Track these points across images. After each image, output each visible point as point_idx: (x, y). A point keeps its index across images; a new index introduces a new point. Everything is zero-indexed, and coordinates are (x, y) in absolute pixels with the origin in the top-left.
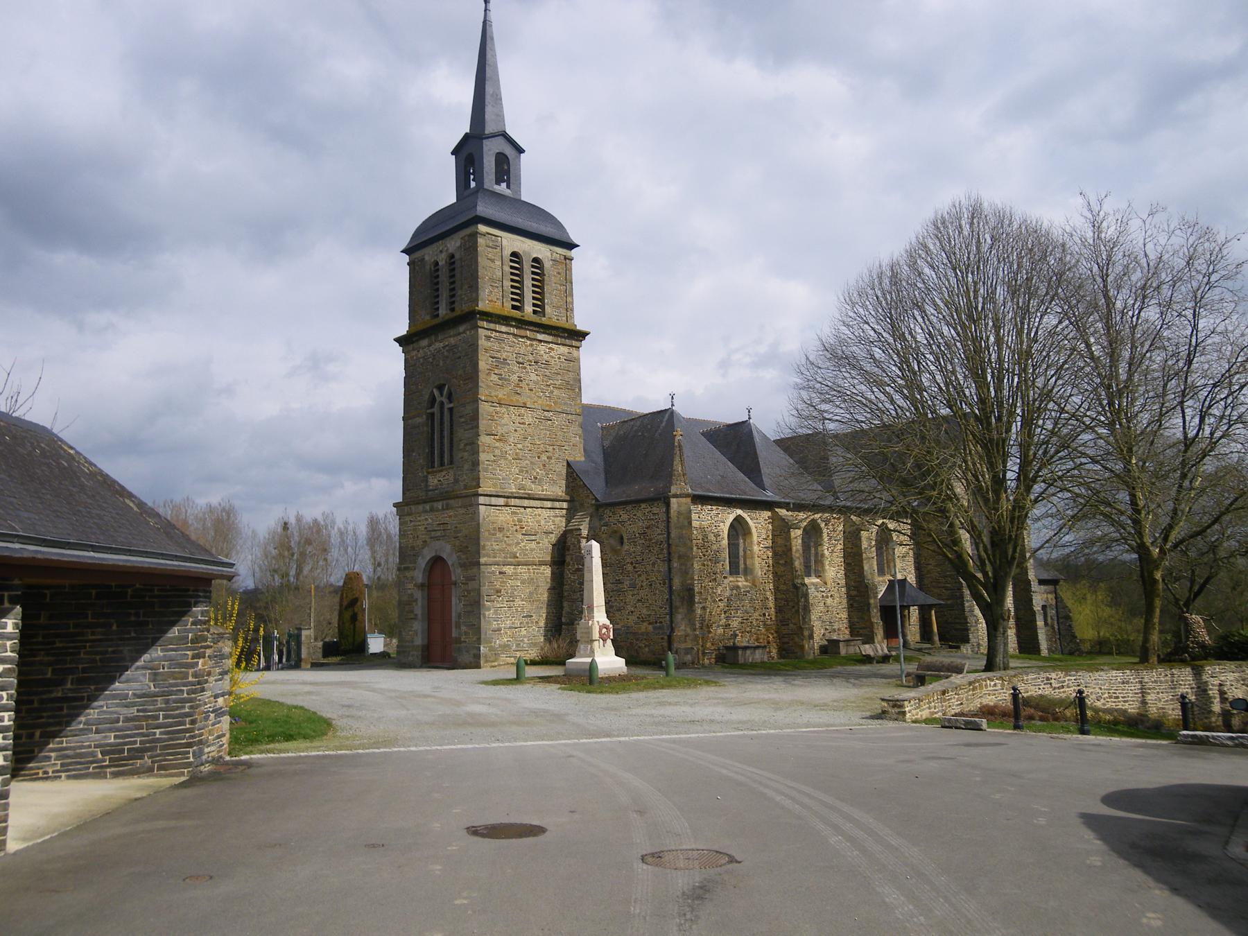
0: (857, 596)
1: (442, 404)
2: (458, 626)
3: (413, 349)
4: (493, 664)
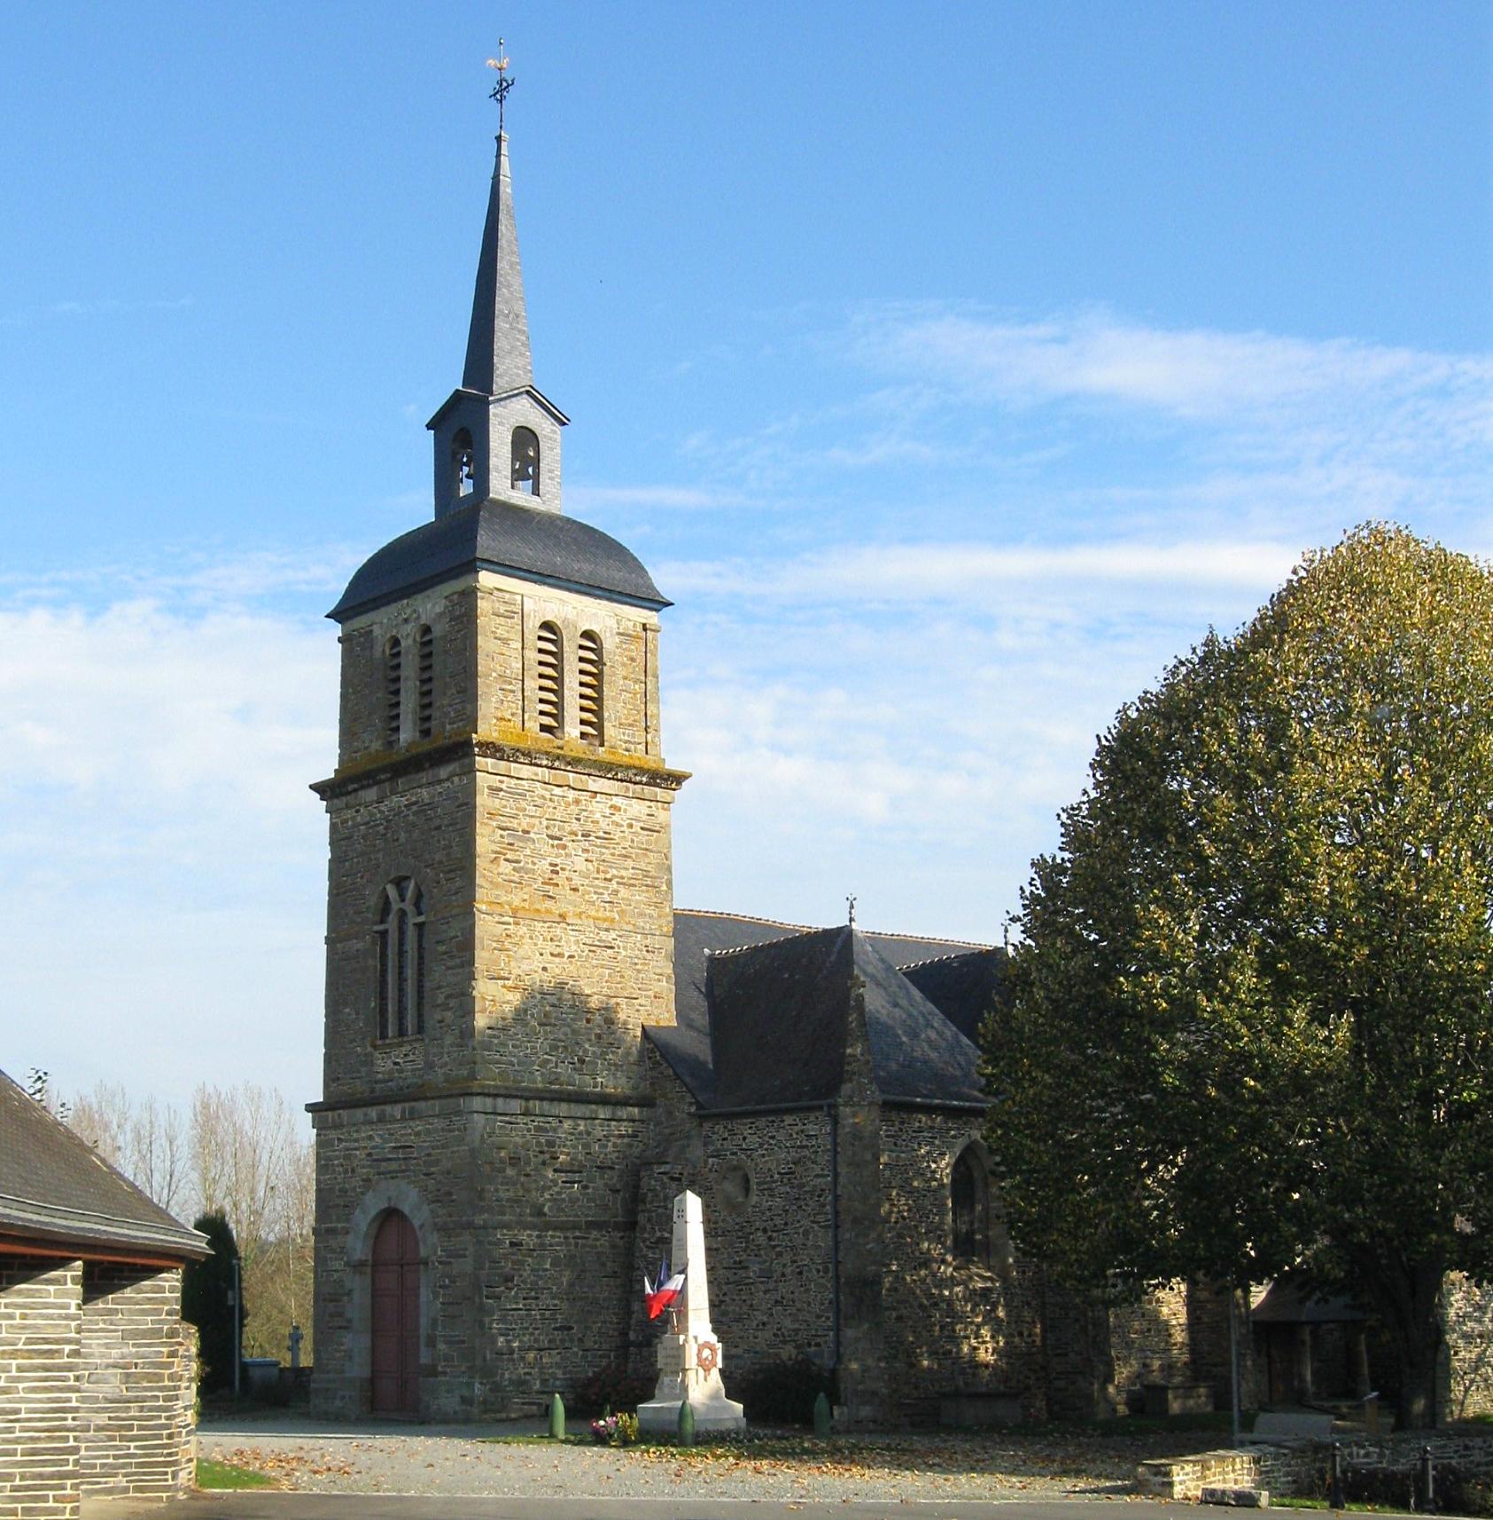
0: (1208, 1301)
1: (402, 913)
2: (432, 1342)
3: (348, 807)
4: (498, 1416)
